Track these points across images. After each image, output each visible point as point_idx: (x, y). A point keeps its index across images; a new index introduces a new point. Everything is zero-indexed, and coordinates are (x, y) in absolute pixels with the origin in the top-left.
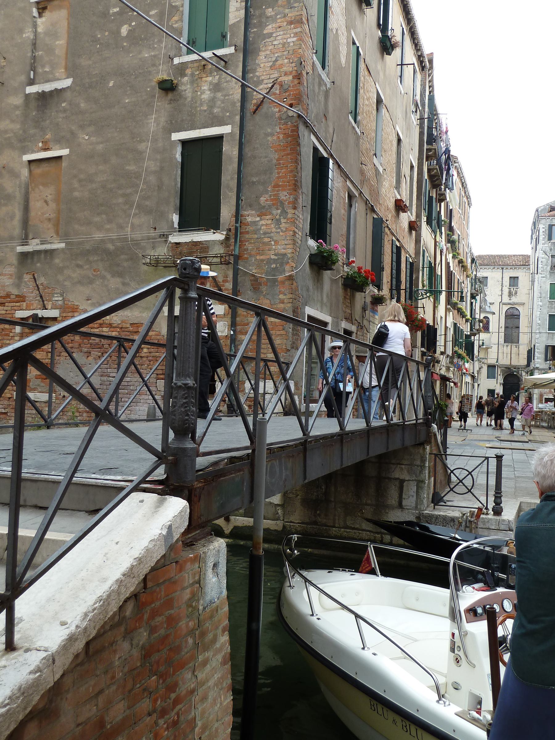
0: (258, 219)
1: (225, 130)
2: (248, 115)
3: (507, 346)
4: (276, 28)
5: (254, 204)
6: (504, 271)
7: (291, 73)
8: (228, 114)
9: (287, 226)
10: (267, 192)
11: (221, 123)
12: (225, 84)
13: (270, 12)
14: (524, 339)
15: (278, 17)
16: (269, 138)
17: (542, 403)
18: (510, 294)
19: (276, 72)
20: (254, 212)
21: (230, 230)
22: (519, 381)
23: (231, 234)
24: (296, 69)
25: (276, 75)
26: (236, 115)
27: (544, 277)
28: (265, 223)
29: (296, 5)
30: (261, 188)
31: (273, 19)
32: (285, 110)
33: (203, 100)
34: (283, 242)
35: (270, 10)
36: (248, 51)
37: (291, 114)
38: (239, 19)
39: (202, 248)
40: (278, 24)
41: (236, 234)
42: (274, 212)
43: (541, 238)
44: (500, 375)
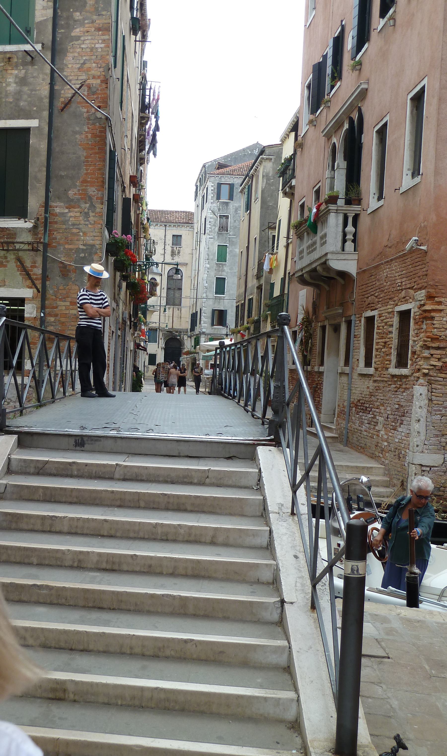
0: (66, 211)
1: (33, 123)
2: (56, 112)
3: (169, 308)
4: (84, 33)
5: (62, 196)
6: (167, 228)
7: (99, 77)
8: (35, 108)
9: (95, 219)
10: (75, 186)
11: (28, 116)
12: (32, 79)
13: (77, 15)
14: (185, 302)
15: (86, 21)
16: (77, 136)
17: (208, 369)
18: (173, 254)
19: (84, 74)
20: (62, 204)
21: (38, 219)
22: (181, 345)
23: (39, 222)
24: (104, 73)
25: (84, 77)
26: (44, 110)
27: (212, 238)
28: (73, 215)
29: (104, 13)
30: (69, 182)
31: (81, 23)
32: (93, 109)
33: (8, 92)
34: (92, 234)
35: (78, 14)
36: (56, 50)
37: (99, 115)
38: (45, 18)
39: (9, 234)
40: (85, 29)
41: (45, 223)
42: (83, 205)
43: (209, 197)
44: (161, 339)
